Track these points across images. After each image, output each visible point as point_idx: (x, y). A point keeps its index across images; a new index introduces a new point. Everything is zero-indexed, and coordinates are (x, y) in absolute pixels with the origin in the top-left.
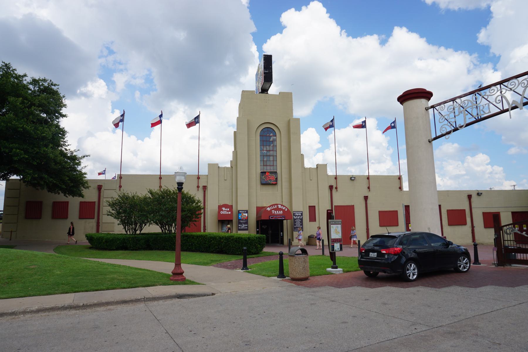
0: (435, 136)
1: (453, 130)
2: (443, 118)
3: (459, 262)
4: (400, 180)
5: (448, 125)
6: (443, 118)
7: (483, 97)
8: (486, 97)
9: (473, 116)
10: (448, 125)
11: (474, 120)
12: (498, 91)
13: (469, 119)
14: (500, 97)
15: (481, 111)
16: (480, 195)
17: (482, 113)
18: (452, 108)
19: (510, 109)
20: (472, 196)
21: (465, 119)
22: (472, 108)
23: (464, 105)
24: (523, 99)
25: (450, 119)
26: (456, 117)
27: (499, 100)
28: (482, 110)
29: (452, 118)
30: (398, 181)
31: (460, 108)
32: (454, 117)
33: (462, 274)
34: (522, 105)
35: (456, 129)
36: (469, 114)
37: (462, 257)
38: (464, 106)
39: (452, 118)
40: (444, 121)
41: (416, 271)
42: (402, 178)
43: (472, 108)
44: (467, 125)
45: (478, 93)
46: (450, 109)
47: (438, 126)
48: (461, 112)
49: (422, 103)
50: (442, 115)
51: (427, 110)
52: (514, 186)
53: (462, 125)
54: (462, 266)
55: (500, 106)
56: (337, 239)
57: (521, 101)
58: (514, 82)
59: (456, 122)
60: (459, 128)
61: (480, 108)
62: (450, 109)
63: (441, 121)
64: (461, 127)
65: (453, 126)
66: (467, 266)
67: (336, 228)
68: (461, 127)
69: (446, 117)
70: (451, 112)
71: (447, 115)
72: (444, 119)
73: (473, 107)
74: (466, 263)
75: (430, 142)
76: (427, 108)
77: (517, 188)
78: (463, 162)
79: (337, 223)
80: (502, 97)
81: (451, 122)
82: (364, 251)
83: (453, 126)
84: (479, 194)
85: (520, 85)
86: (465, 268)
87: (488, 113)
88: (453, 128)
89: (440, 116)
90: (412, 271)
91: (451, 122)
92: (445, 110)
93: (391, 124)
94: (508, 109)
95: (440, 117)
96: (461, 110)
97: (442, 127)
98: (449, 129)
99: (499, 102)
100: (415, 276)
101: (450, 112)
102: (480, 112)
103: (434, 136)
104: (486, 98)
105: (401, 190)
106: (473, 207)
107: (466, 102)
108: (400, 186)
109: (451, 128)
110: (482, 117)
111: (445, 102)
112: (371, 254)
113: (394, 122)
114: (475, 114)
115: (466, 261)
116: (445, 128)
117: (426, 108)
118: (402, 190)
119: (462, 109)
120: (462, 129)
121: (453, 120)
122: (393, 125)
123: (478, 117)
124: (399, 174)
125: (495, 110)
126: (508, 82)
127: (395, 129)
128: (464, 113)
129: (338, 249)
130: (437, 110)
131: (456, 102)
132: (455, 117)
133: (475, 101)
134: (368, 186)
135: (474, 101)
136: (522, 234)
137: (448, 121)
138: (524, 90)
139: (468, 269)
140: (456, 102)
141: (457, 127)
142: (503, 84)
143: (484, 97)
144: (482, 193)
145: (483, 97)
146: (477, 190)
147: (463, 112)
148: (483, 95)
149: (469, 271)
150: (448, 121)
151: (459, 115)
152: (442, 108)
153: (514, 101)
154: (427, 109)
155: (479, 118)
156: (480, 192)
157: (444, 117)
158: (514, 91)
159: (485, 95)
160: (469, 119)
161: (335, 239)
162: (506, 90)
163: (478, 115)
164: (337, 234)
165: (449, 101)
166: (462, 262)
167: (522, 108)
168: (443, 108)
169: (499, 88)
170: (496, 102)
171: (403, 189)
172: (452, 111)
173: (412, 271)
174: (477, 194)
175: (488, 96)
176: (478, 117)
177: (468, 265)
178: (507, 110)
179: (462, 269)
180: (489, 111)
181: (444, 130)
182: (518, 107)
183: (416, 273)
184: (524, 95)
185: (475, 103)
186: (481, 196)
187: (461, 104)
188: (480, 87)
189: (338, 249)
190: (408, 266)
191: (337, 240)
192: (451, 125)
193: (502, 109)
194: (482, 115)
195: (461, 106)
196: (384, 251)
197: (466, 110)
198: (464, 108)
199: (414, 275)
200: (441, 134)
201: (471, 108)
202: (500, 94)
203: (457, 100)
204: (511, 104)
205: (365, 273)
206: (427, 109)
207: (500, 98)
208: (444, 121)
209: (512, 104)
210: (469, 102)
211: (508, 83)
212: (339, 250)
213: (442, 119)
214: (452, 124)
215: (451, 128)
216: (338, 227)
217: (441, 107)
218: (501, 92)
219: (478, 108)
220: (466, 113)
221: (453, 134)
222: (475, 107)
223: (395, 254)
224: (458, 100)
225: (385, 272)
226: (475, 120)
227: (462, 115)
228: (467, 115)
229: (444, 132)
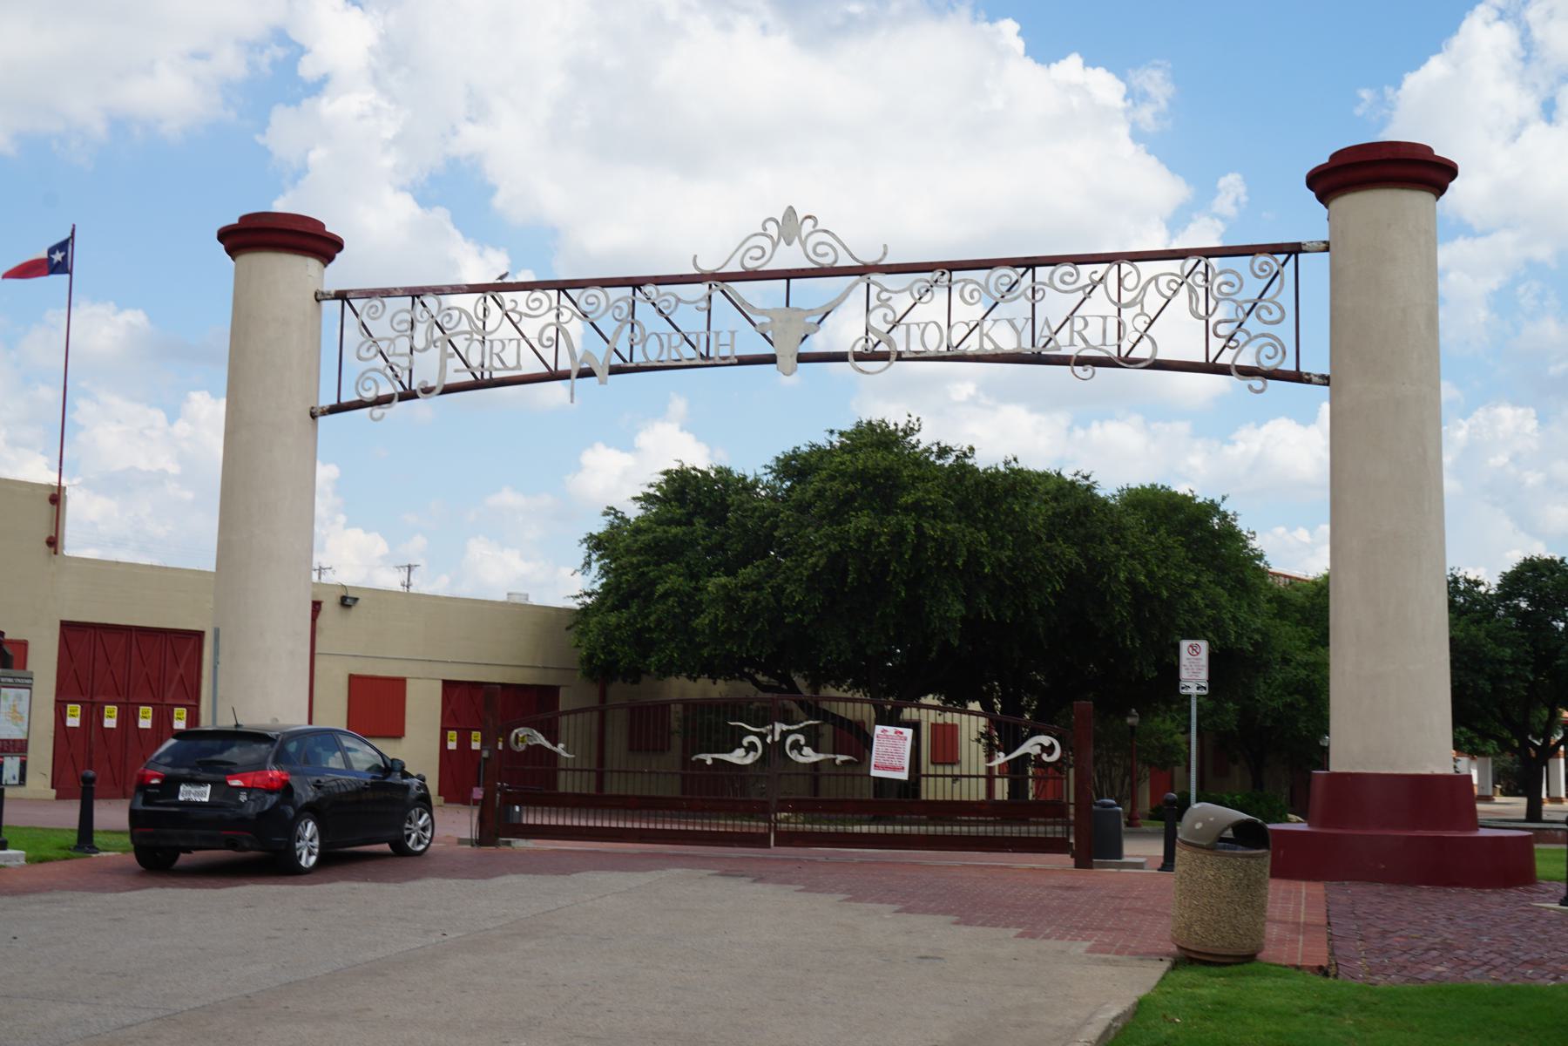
0: (335, 402)
1: (399, 394)
2: (371, 346)
3: (407, 825)
4: (55, 507)
5: (386, 376)
6: (371, 346)
7: (507, 315)
8: (515, 317)
9: (468, 367)
10: (386, 376)
11: (467, 377)
12: (550, 309)
13: (456, 371)
14: (553, 329)
15: (495, 357)
16: (349, 606)
17: (497, 363)
18: (406, 321)
19: (574, 374)
20: (323, 605)
21: (443, 367)
22: (471, 340)
23: (447, 322)
24: (611, 354)
25: (394, 354)
26: (414, 352)
27: (549, 339)
28: (498, 355)
29: (401, 355)
30: (47, 508)
31: (433, 329)
32: (408, 351)
33: (416, 858)
34: (607, 370)
35: (408, 395)
36: (456, 355)
37: (418, 809)
38: (446, 326)
39: (401, 355)
40: (376, 355)
41: (316, 842)
42: (65, 497)
43: (471, 340)
44: (449, 390)
45: (493, 297)
46: (401, 322)
47: (352, 366)
48: (435, 342)
49: (301, 270)
50: (370, 335)
51: (318, 301)
52: (409, 567)
53: (430, 385)
54: (414, 836)
55: (549, 355)
56: (14, 741)
57: (604, 359)
58: (596, 297)
59: (411, 371)
60: (420, 394)
61: (492, 347)
62: (401, 322)
63: (363, 353)
64: (427, 391)
65: (401, 383)
66: (425, 838)
67: (16, 703)
68: (427, 391)
69: (384, 346)
70: (401, 333)
71: (389, 339)
72: (373, 350)
73: (472, 336)
74: (424, 829)
75: (313, 416)
76: (323, 293)
77: (421, 586)
78: (173, 416)
79: (19, 680)
80: (557, 330)
81: (398, 366)
82: (155, 781)
83: (401, 383)
84: (346, 602)
85: (610, 312)
86: (419, 842)
87: (513, 369)
88: (401, 389)
89: (363, 334)
90: (308, 842)
91: (398, 366)
92: (387, 318)
93: (52, 251)
94: (570, 371)
95: (363, 339)
96: (435, 337)
97: (363, 374)
98: (386, 389)
99: (550, 343)
100: (313, 859)
101: (399, 331)
102: (491, 359)
103: (329, 399)
104: (515, 320)
105: (56, 553)
106: (318, 650)
107: (455, 314)
108: (53, 535)
109: (395, 387)
110: (496, 375)
111: (387, 293)
112: (183, 788)
113: (63, 246)
114: (475, 361)
115: (426, 820)
116: (375, 381)
117: (316, 294)
118: (59, 550)
119: (437, 332)
120: (426, 398)
121: (404, 362)
122: (58, 257)
123: (482, 374)
124: (57, 480)
125: (532, 366)
126: (581, 290)
127: (67, 276)
128: (444, 350)
129: (14, 778)
130: (357, 315)
131: (423, 303)
132: (411, 353)
133: (481, 320)
134: (46, 532)
135: (478, 318)
136: (554, 748)
137: (386, 360)
138: (617, 330)
139: (428, 846)
140: (423, 303)
141: (413, 387)
142: (567, 291)
143: (509, 313)
144: (356, 599)
145: (507, 315)
146: (343, 586)
147: (438, 344)
148: (507, 308)
149: (425, 853)
150: (386, 360)
151: (425, 349)
152: (373, 310)
153: (587, 354)
154: (319, 297)
155: (487, 376)
156: (351, 594)
157: (374, 342)
158: (592, 324)
159: (513, 310)
160: (456, 371)
161: (8, 741)
162: (574, 314)
163: (483, 366)
164: (17, 725)
165: (400, 294)
166: (415, 825)
167: (606, 379)
168: (377, 311)
169: (555, 304)
170: (540, 341)
171: (63, 548)
172: (406, 331)
173: (308, 842)
174: (339, 600)
175: (521, 314)
176: (482, 374)
177: (428, 834)
178: (565, 376)
179: (413, 846)
180: (518, 362)
181: (370, 389)
182: (597, 374)
183: (316, 850)
184: (615, 344)
185: (480, 325)
186: (354, 608)
187: (437, 315)
188: (501, 277)
189: (14, 778)
190: (413, 812)
191: (14, 746)
192: (397, 376)
193: (553, 368)
194: (496, 369)
195: (437, 323)
196: (237, 779)
197: (450, 341)
198: (444, 333)
199: (310, 854)
200: (358, 398)
201: (466, 339)
202: (554, 321)
203: (426, 300)
204: (578, 360)
205: (138, 861)
206: (319, 297)
207: (551, 332)
208: (376, 355)
209: (582, 362)
210: (464, 317)
211: (582, 293)
212: (16, 782)
213: (368, 349)
214: (399, 375)
215: (395, 387)
216: (19, 698)
217: (371, 307)
218: (558, 316)
219: (487, 343)
220: (450, 349)
221: (398, 406)
222: (478, 340)
223: (271, 791)
224: (430, 300)
225: (232, 845)
226: (473, 379)
227: (435, 353)
228: (452, 356)
229: (369, 395)
